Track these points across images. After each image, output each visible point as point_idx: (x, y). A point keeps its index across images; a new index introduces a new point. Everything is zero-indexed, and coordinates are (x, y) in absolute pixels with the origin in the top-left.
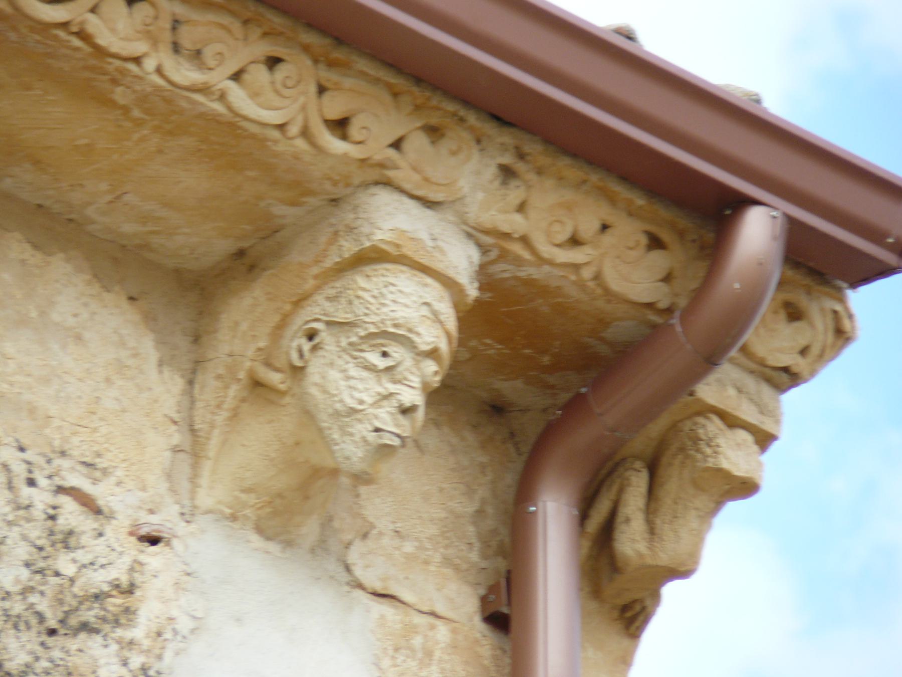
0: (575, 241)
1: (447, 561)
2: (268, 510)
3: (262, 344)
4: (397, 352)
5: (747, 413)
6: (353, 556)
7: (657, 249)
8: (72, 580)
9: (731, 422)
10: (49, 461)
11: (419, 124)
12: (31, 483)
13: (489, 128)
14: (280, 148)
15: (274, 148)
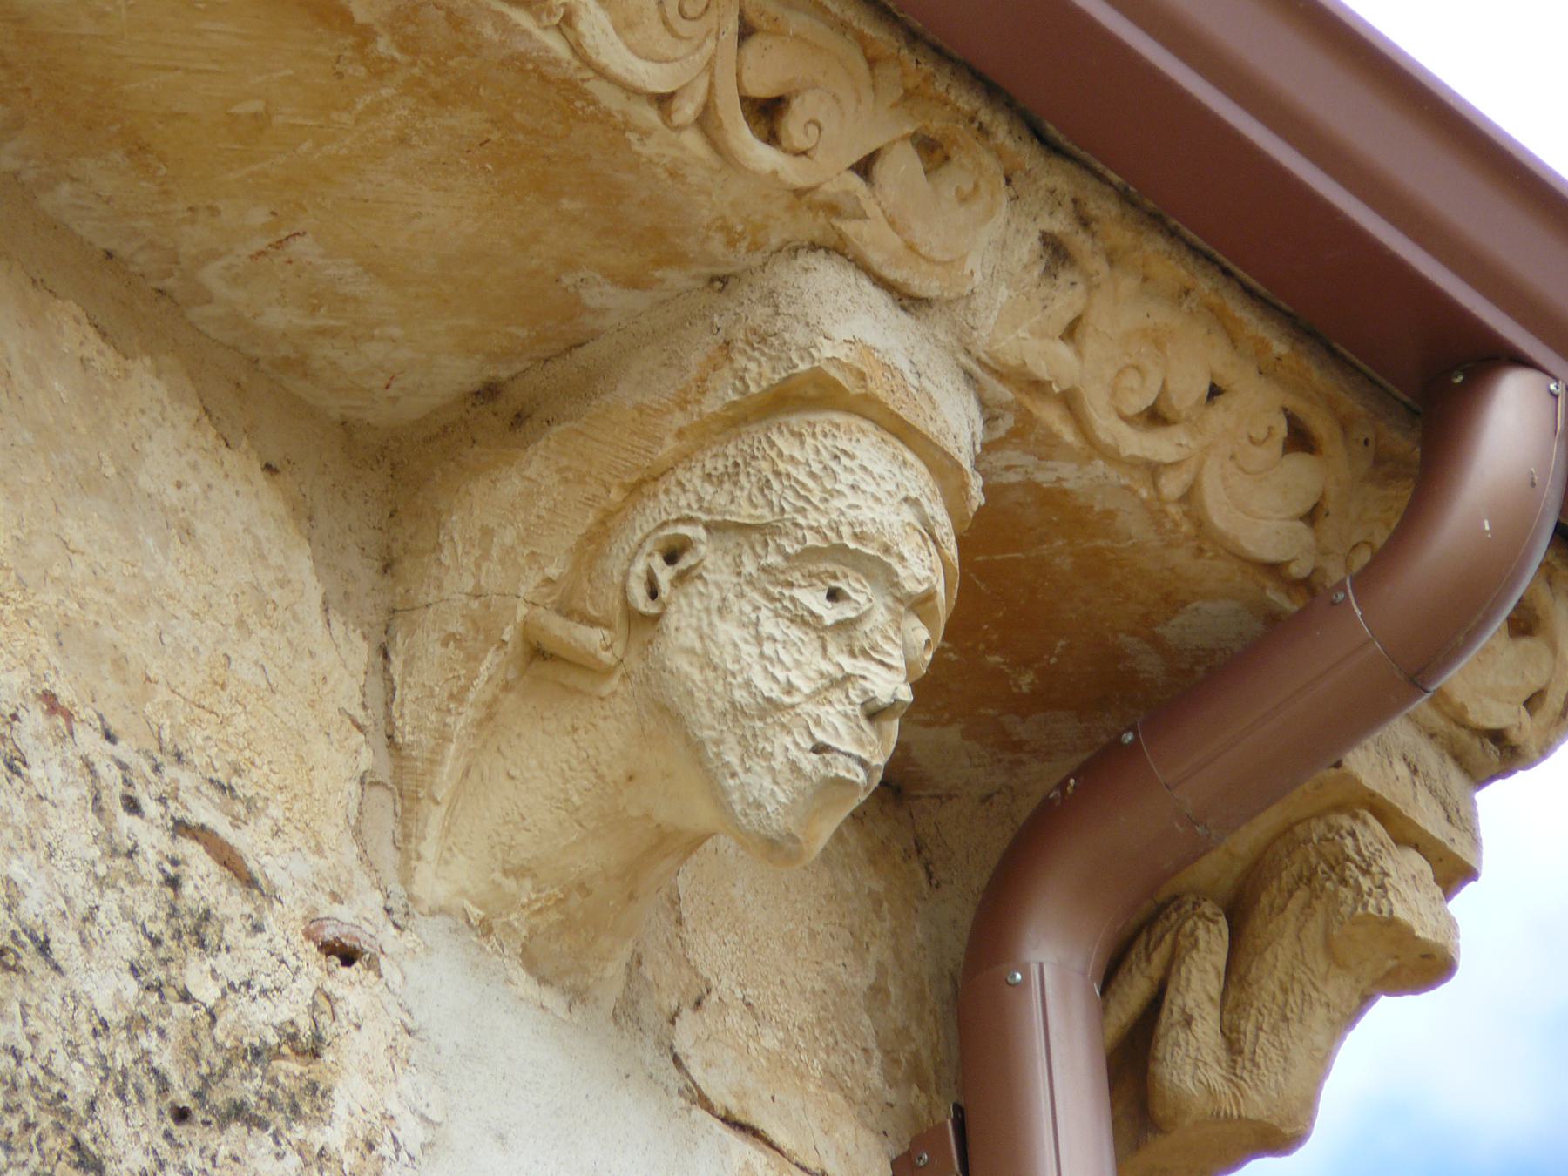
0: (1155, 417)
1: (832, 1078)
2: (554, 916)
3: (553, 571)
4: (861, 593)
5: (1428, 818)
6: (684, 1039)
7: (1298, 451)
8: (213, 1015)
9: (1406, 835)
10: (157, 769)
11: (909, 129)
12: (132, 806)
13: (1028, 155)
14: (650, 149)
15: (637, 147)
